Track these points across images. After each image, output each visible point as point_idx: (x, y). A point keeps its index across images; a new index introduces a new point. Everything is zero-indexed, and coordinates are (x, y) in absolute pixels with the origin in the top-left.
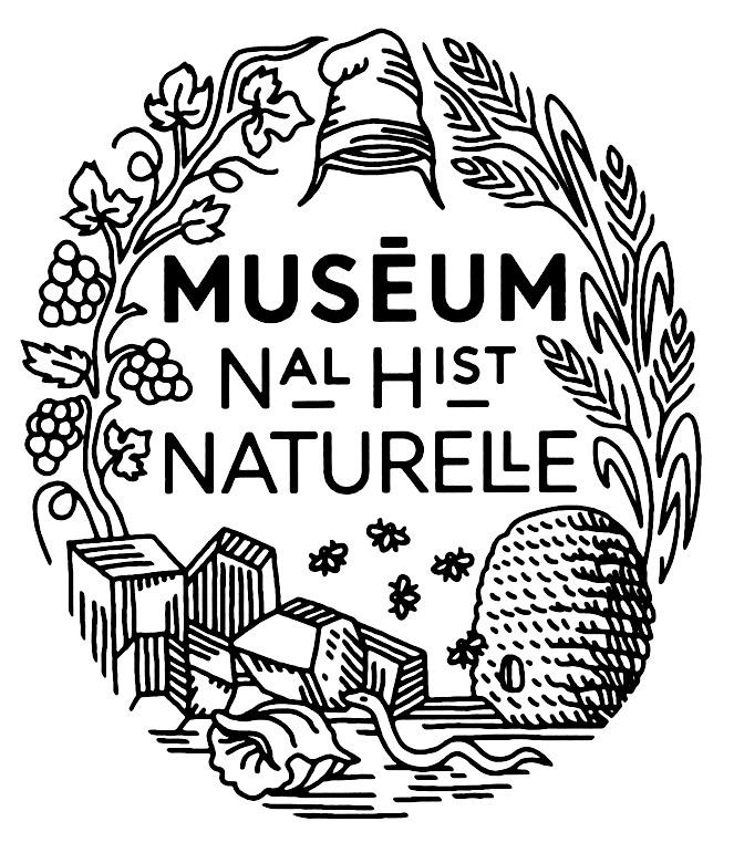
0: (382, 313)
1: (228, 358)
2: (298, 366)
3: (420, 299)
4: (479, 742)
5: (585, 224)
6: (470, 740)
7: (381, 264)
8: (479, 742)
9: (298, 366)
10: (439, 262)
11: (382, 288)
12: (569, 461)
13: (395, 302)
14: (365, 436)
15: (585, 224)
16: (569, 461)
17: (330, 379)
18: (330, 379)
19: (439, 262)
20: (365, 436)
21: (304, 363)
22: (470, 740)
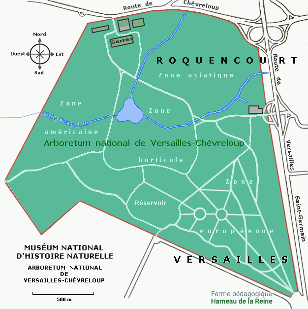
0: (43, 250)
1: (68, 255)
2: (227, 259)
3: (46, 249)
4: (246, 33)
5: (278, 126)
6: (247, 36)
7: (43, 246)
8: (246, 33)
9: (227, 259)
10: (48, 246)
11: (43, 247)
12: (105, 254)
13: (44, 249)
14: (197, 58)
15: (278, 126)
16: (105, 254)
17: (100, 250)
18: (100, 250)
19: (48, 246)
20: (197, 58)
21: (228, 259)
22: (247, 36)
